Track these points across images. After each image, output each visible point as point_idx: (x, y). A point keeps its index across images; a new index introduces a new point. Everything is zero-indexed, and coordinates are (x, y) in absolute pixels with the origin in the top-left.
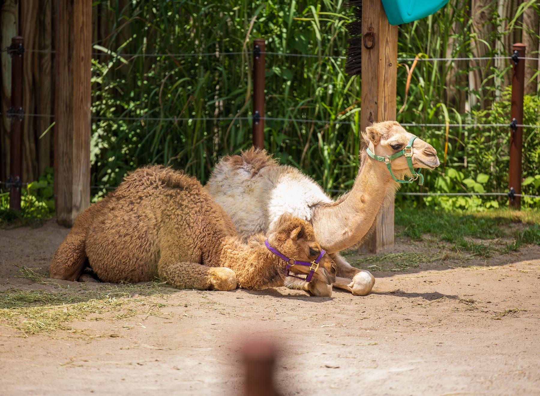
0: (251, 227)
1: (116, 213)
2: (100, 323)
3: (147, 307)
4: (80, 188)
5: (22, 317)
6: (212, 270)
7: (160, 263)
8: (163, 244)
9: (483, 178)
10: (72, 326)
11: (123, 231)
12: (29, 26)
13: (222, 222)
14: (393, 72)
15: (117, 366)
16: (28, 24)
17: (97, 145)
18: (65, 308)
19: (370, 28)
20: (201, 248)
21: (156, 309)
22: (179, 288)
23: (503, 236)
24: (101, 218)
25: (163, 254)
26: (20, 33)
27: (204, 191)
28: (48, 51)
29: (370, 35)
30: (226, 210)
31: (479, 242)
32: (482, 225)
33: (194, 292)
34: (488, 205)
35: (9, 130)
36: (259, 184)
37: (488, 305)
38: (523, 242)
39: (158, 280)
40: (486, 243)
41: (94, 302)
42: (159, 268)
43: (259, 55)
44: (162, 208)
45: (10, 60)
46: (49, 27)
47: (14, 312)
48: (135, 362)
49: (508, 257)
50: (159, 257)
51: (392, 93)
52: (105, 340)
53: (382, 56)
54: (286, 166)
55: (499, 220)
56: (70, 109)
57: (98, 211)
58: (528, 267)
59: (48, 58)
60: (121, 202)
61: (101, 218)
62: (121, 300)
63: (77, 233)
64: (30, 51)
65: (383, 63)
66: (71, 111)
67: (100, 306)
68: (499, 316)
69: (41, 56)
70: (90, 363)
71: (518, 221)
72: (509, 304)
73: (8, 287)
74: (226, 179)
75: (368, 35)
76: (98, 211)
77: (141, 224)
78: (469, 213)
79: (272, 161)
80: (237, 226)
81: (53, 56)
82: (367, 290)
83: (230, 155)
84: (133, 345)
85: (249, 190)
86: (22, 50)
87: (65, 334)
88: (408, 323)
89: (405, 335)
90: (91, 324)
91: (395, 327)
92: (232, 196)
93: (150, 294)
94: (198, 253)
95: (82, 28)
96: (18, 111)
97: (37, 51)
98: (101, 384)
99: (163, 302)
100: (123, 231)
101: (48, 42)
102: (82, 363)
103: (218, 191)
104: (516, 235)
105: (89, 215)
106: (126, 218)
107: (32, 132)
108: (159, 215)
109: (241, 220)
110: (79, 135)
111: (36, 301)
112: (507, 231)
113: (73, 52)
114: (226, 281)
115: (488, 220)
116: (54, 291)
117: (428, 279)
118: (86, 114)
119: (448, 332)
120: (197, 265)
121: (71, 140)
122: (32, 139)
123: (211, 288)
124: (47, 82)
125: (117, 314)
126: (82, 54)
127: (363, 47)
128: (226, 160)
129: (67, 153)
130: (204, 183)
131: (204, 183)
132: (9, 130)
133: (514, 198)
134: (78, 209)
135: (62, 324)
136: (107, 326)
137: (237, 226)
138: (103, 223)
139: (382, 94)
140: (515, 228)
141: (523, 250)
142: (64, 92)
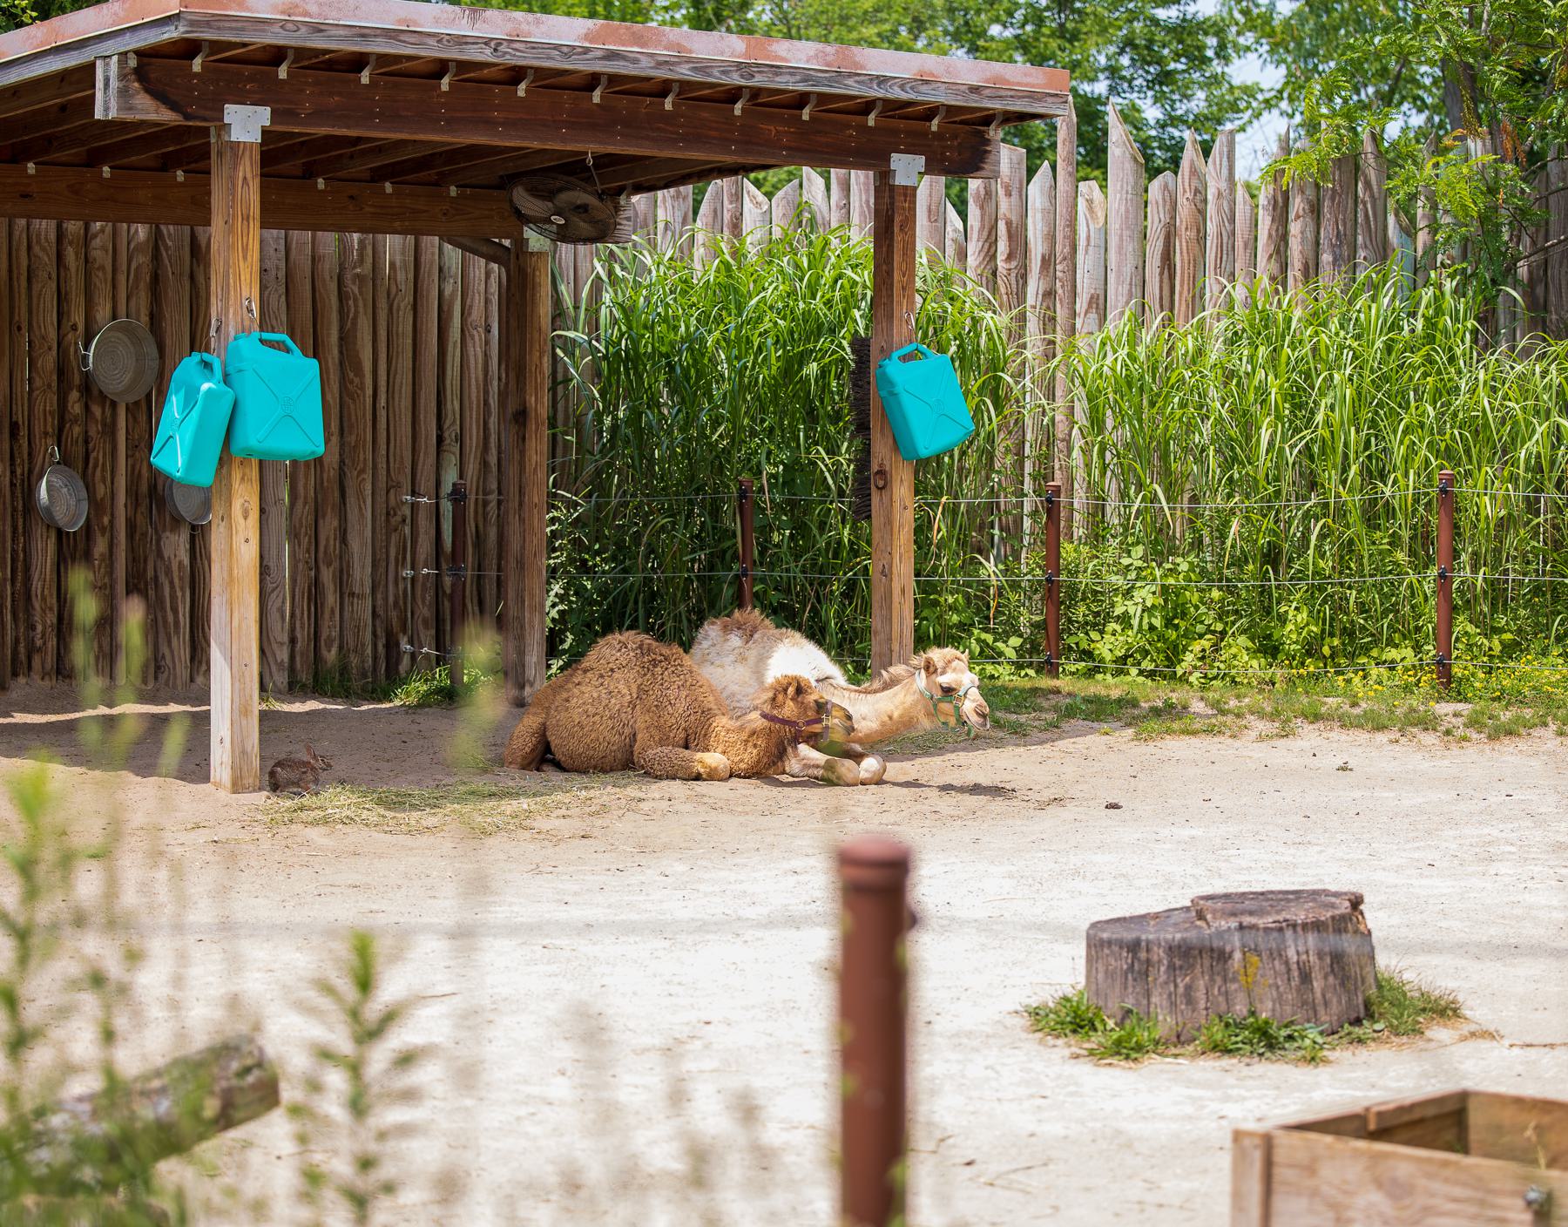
0: (746, 703)
1: (583, 688)
2: (568, 820)
3: (623, 801)
4: (534, 659)
5: (475, 814)
6: (699, 755)
7: (637, 748)
8: (640, 725)
9: (1015, 641)
10: (535, 824)
11: (592, 710)
12: (472, 468)
13: (711, 698)
14: (909, 515)
15: (593, 872)
16: (471, 466)
17: (554, 606)
18: (524, 803)
19: (881, 465)
20: (685, 729)
21: (634, 804)
22: (659, 778)
23: (1041, 709)
24: (565, 695)
25: (639, 737)
26: (461, 477)
27: (686, 657)
28: (493, 497)
29: (881, 473)
30: (714, 682)
31: (1014, 717)
32: (1016, 697)
33: (678, 782)
34: (1023, 673)
35: (448, 591)
36: (752, 653)
37: (1029, 793)
38: (1065, 716)
39: (634, 769)
40: (1023, 718)
41: (559, 796)
42: (636, 754)
43: (746, 498)
44: (639, 682)
45: (451, 508)
46: (494, 469)
47: (468, 808)
48: (613, 867)
49: (1049, 735)
50: (635, 741)
51: (909, 541)
52: (577, 841)
53: (896, 497)
54: (784, 630)
55: (1035, 691)
56: (521, 564)
57: (561, 687)
58: (1071, 746)
59: (493, 504)
60: (589, 675)
61: (565, 695)
62: (592, 793)
63: (535, 714)
64: (473, 497)
65: (897, 505)
66: (522, 568)
67: (567, 801)
68: (1042, 806)
69: (486, 503)
70: (560, 869)
71: (1057, 692)
72: (1053, 790)
73: (457, 779)
74: (714, 645)
75: (878, 472)
76: (561, 687)
77: (613, 701)
78: (999, 683)
79: (767, 622)
80: (728, 702)
81: (499, 503)
82: (876, 778)
83: (716, 617)
84: (610, 848)
85: (742, 659)
86: (465, 497)
87: (527, 834)
88: (937, 816)
89: (934, 830)
90: (557, 822)
91: (1407, 846)
92: (722, 666)
93: (625, 786)
94: (683, 735)
95: (535, 469)
96: (460, 569)
97: (481, 497)
98: (575, 894)
99: (642, 795)
100: (592, 710)
101: (494, 486)
102: (551, 869)
103: (704, 660)
104: (1056, 709)
105: (549, 691)
106: (595, 695)
107: (475, 593)
108: (634, 690)
109: (734, 695)
110: (532, 596)
111: (492, 795)
112: (1045, 704)
113: (444, 625)
114: (716, 768)
115: (1022, 691)
116: (511, 784)
117: (956, 763)
118: (540, 571)
119: (985, 826)
120: (681, 750)
121: (523, 602)
122: (475, 601)
123: (698, 777)
124: (492, 533)
125: (588, 810)
126: (536, 500)
127: (873, 487)
128: (713, 623)
129: (518, 618)
130: (686, 651)
131: (686, 651)
132: (448, 591)
133: (1052, 664)
134: (532, 685)
135: (524, 823)
136: (576, 825)
137: (728, 702)
138: (567, 701)
139: (896, 543)
140: (1054, 699)
141: (1065, 726)
142: (514, 545)
